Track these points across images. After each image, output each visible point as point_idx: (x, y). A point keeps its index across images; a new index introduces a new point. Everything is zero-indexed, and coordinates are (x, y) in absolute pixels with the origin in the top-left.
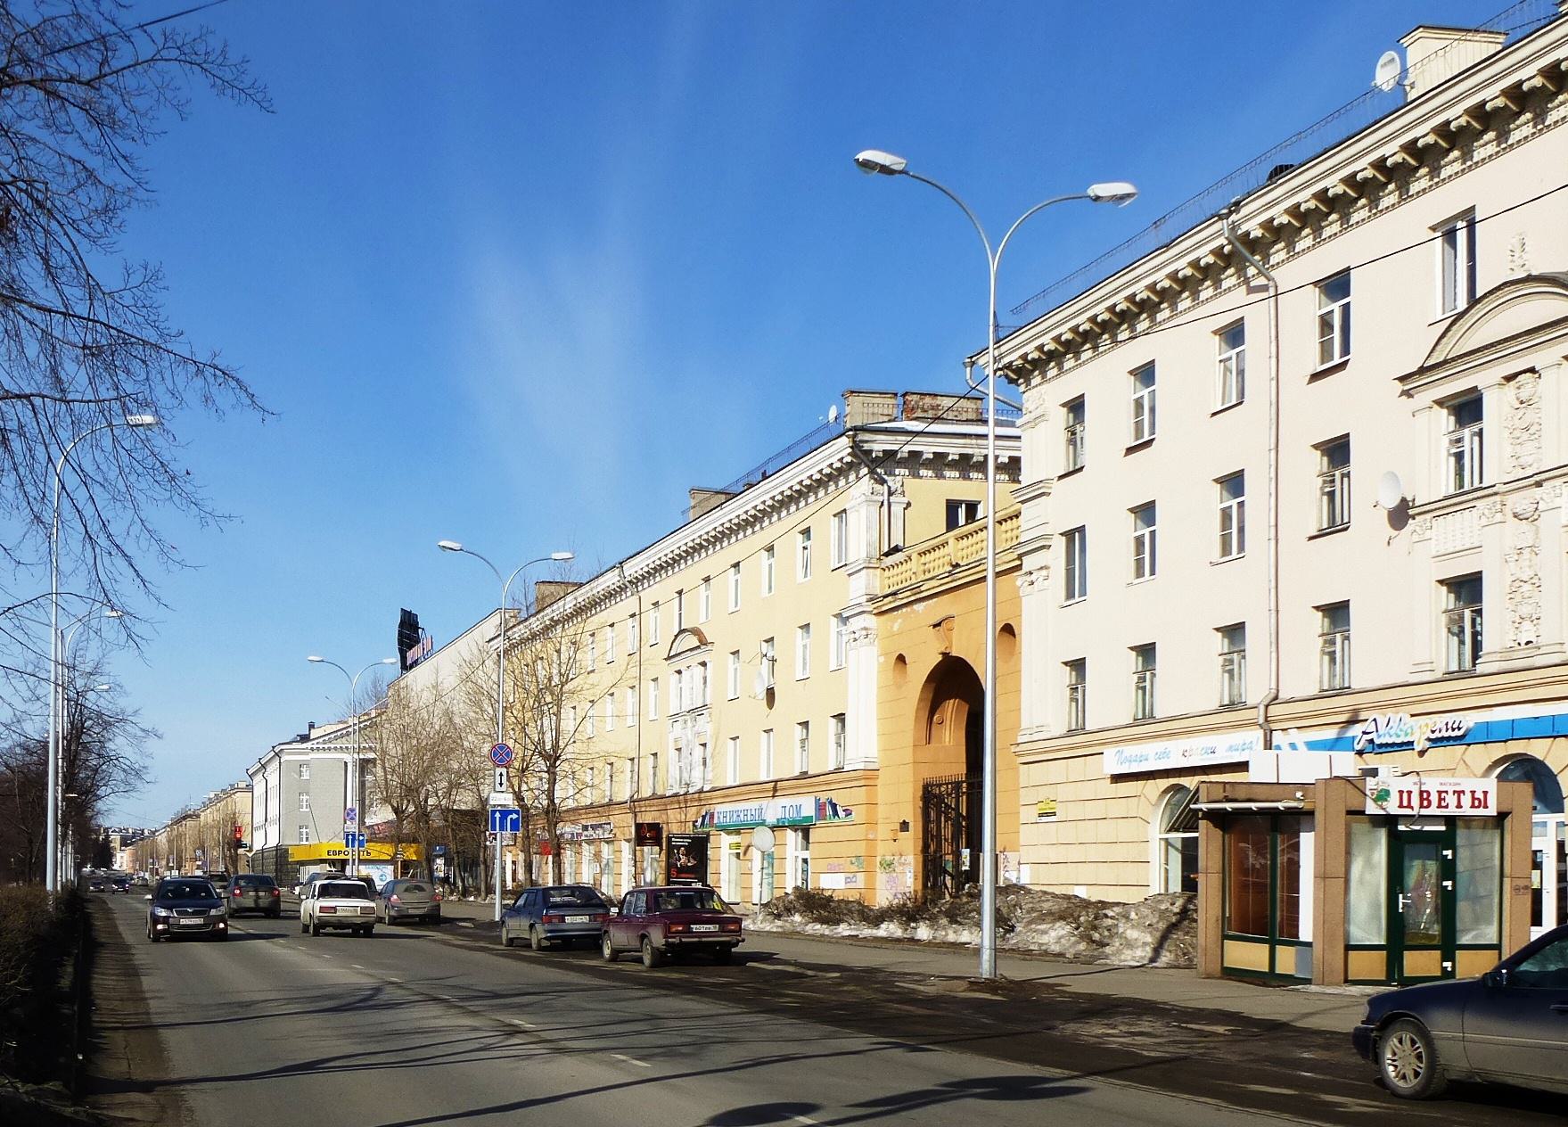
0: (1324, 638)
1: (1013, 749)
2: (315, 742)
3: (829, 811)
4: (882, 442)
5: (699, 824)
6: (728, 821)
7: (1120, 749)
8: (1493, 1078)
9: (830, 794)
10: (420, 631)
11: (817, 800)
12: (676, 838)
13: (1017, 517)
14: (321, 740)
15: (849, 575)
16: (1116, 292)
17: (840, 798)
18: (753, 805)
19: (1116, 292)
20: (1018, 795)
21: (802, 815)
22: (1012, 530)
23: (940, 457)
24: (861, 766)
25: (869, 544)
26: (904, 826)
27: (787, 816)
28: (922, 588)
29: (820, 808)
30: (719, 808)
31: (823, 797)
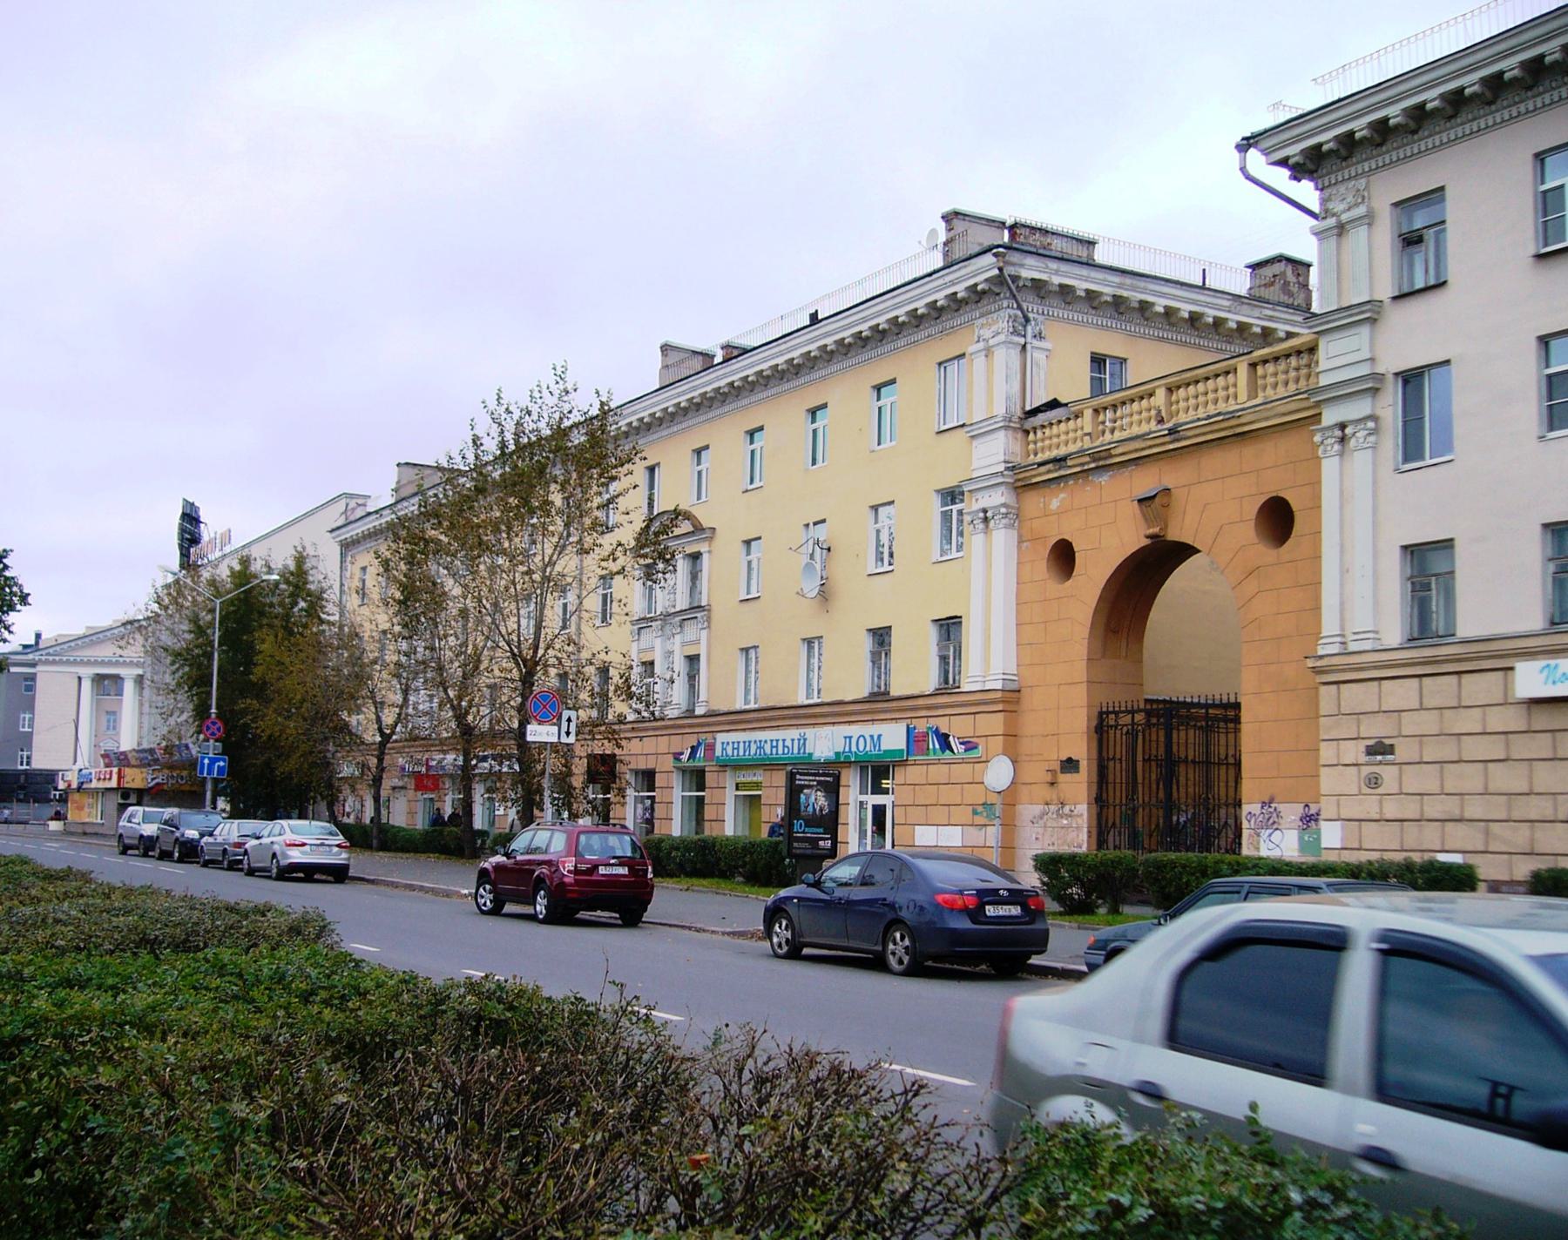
0: (1559, 562)
1: (1310, 663)
2: (44, 652)
3: (933, 743)
4: (1031, 268)
5: (685, 757)
6: (741, 753)
7: (1552, 662)
8: (195, 810)
9: (933, 722)
10: (202, 526)
11: (908, 726)
12: (801, 774)
13: (1151, 395)
14: (51, 651)
15: (973, 437)
16: (880, 314)
17: (958, 728)
18: (793, 734)
19: (880, 314)
20: (1318, 726)
21: (883, 748)
22: (1059, 436)
23: (1091, 295)
24: (999, 685)
25: (1008, 398)
26: (1070, 765)
27: (854, 749)
28: (1113, 452)
29: (915, 741)
30: (721, 738)
31: (921, 726)
